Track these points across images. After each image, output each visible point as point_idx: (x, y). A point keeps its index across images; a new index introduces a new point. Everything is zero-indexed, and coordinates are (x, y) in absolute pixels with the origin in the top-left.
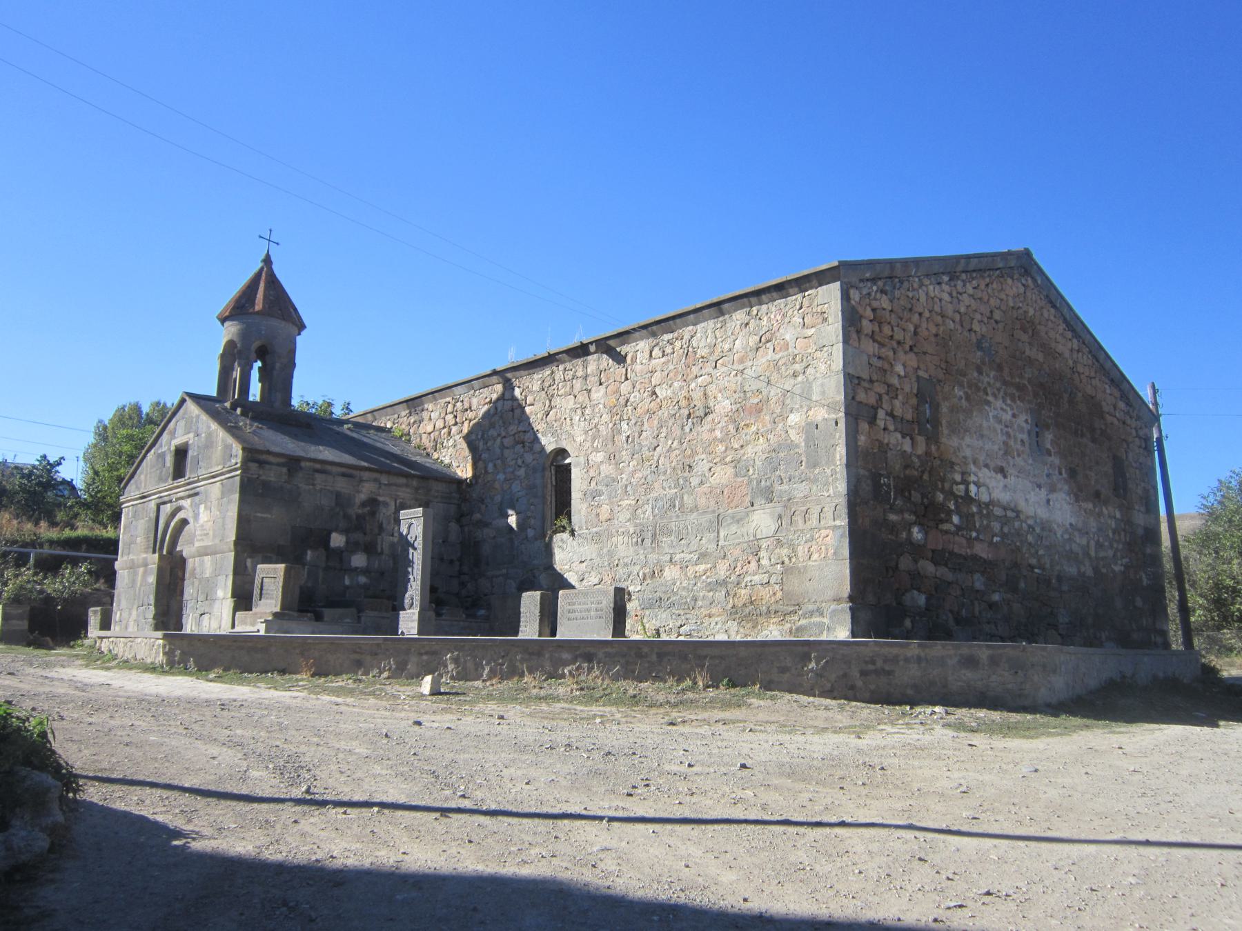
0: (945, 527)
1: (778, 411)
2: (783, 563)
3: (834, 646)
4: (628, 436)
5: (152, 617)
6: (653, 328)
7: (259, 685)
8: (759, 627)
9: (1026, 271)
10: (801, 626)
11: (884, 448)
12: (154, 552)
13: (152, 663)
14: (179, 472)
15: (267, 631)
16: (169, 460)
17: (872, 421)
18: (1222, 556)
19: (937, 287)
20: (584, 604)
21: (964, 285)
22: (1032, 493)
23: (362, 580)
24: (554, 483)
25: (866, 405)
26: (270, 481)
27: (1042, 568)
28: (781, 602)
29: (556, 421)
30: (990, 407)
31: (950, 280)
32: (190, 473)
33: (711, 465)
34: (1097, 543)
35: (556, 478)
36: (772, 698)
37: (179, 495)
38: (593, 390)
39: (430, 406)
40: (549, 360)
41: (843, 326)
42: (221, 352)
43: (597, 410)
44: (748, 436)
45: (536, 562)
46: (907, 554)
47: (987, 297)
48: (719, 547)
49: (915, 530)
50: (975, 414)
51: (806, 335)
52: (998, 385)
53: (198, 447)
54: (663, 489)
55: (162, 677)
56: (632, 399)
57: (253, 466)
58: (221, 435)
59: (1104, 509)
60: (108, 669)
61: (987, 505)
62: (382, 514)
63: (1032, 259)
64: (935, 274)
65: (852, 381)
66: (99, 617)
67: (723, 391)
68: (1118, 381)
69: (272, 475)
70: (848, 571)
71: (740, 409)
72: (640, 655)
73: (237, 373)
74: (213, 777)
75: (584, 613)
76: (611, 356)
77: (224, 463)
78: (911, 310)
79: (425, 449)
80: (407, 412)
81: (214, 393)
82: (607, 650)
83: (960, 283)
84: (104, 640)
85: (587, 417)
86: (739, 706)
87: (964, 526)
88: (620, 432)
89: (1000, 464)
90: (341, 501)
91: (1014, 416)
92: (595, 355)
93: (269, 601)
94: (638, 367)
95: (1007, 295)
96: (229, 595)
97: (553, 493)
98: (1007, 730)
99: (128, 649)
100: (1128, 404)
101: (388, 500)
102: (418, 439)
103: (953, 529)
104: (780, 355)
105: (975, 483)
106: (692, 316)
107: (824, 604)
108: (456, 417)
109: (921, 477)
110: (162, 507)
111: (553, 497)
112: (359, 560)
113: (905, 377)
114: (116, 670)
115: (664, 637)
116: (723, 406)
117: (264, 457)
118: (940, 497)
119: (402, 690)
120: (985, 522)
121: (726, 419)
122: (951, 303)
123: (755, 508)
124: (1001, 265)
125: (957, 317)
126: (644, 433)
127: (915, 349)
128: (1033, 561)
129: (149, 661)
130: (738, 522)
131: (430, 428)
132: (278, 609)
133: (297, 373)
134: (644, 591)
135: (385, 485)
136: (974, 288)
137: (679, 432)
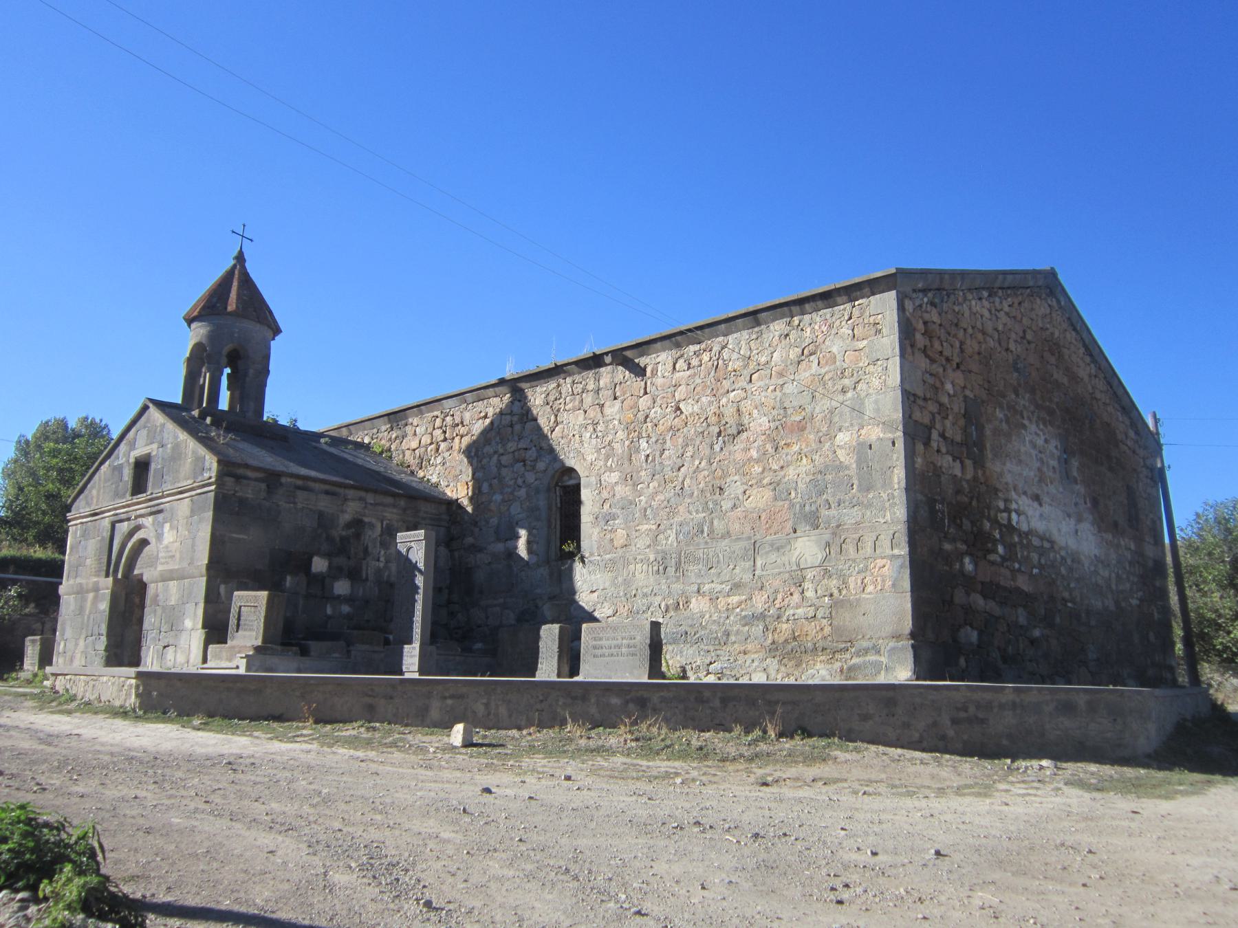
0: (992, 557)
1: (824, 429)
2: (831, 595)
3: (922, 690)
4: (648, 456)
5: (103, 648)
6: (676, 339)
7: (256, 734)
8: (804, 666)
9: (1051, 291)
10: (854, 665)
11: (937, 471)
12: (107, 575)
13: (121, 707)
14: (139, 486)
15: (248, 668)
16: (128, 474)
17: (927, 444)
18: (1202, 589)
19: (979, 302)
20: (613, 639)
21: (1001, 303)
22: (1064, 522)
23: (346, 609)
24: (559, 505)
25: (921, 424)
26: (247, 498)
27: (1073, 601)
28: (830, 638)
29: (562, 438)
30: (1026, 430)
31: (990, 296)
32: (153, 488)
33: (746, 487)
34: (1118, 575)
35: (561, 500)
36: (856, 750)
37: (138, 512)
38: (607, 404)
39: (415, 421)
40: (556, 371)
41: (899, 338)
42: (188, 355)
43: (611, 426)
44: (789, 457)
45: (538, 591)
46: (961, 587)
47: (1020, 316)
48: (756, 577)
49: (967, 560)
50: (1014, 438)
51: (857, 348)
52: (1032, 408)
53: (163, 459)
54: (690, 513)
55: (140, 724)
56: (652, 415)
57: (229, 481)
58: (191, 445)
60: (69, 712)
61: (1027, 534)
62: (367, 537)
63: (1057, 279)
64: (976, 289)
65: (909, 398)
66: (38, 647)
67: (760, 408)
68: (1128, 408)
69: (252, 491)
70: (909, 606)
71: (780, 427)
72: (701, 700)
73: (206, 379)
74: (286, 886)
75: (612, 650)
76: (626, 367)
77: (195, 477)
78: (957, 325)
79: (409, 466)
80: (388, 426)
81: (179, 400)
82: (662, 694)
83: (997, 300)
84: (60, 677)
85: (600, 434)
86: (824, 760)
87: (1007, 557)
88: (638, 450)
89: (1036, 492)
90: (324, 521)
91: (1046, 441)
92: (609, 367)
93: (247, 633)
94: (659, 381)
95: (1037, 315)
96: (200, 625)
97: (558, 515)
98: (1136, 788)
99: (90, 689)
100: (1137, 433)
101: (374, 521)
102: (401, 456)
103: (999, 559)
104: (827, 368)
105: (1016, 511)
107: (881, 641)
108: (445, 432)
109: (970, 503)
110: (117, 525)
111: (558, 523)
112: (342, 587)
113: (954, 396)
114: (78, 714)
115: (692, 679)
116: (760, 423)
117: (241, 471)
118: (987, 525)
119: (431, 741)
120: (1025, 553)
121: (763, 437)
122: (990, 320)
124: (1031, 283)
125: (996, 336)
126: (667, 452)
127: (962, 368)
128: (1066, 595)
129: (117, 703)
130: (778, 549)
131: (414, 444)
132: (259, 642)
133: (270, 381)
134: (667, 624)
135: (371, 504)
136: (1009, 306)
137: (707, 451)
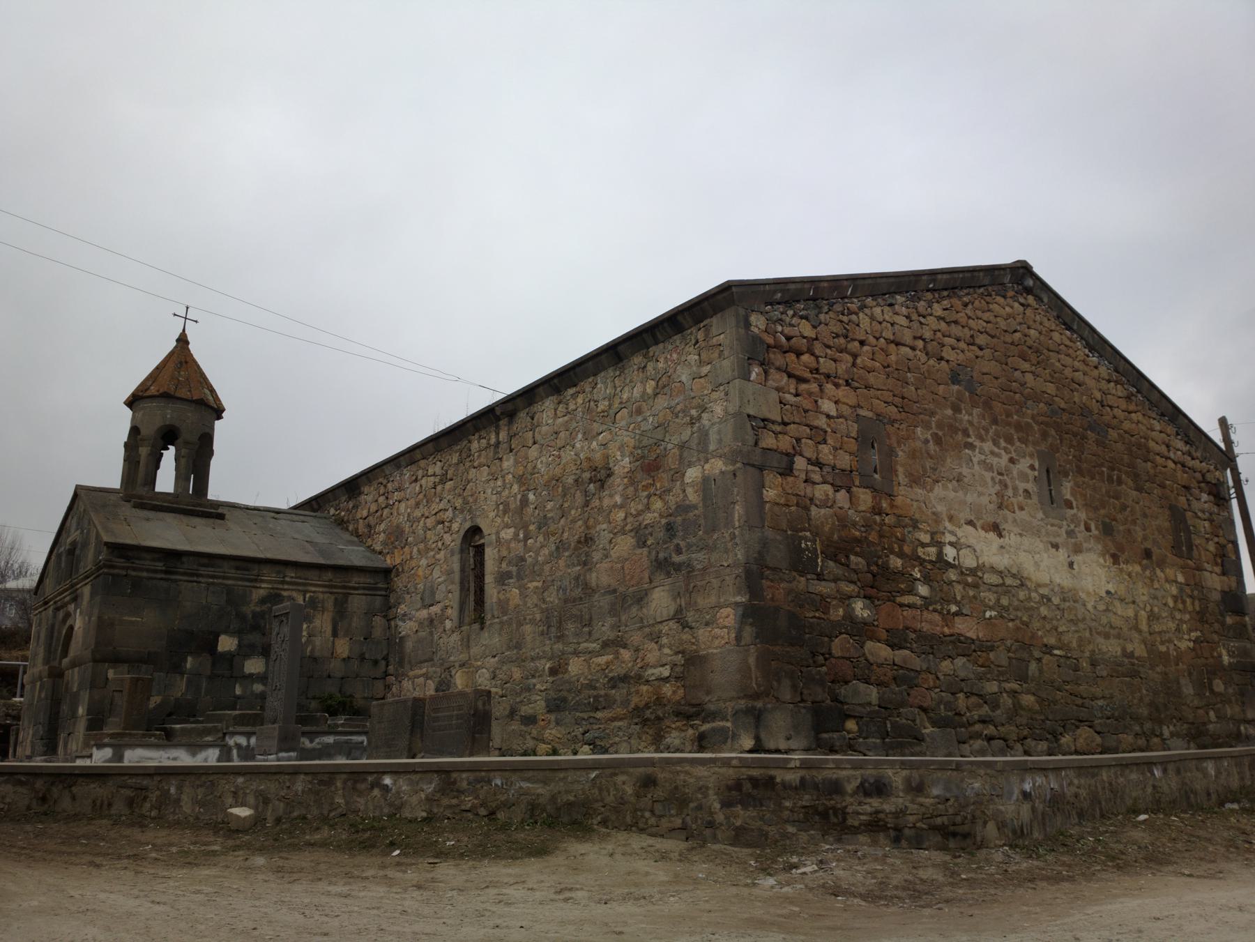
0: (907, 599)
11: (805, 504)
24: (122, 560)
59: (1158, 571)
61: (973, 572)
91: (1012, 461)
105: (951, 544)
106: (590, 363)
118: (896, 562)
123: (654, 584)
128: (1052, 641)
